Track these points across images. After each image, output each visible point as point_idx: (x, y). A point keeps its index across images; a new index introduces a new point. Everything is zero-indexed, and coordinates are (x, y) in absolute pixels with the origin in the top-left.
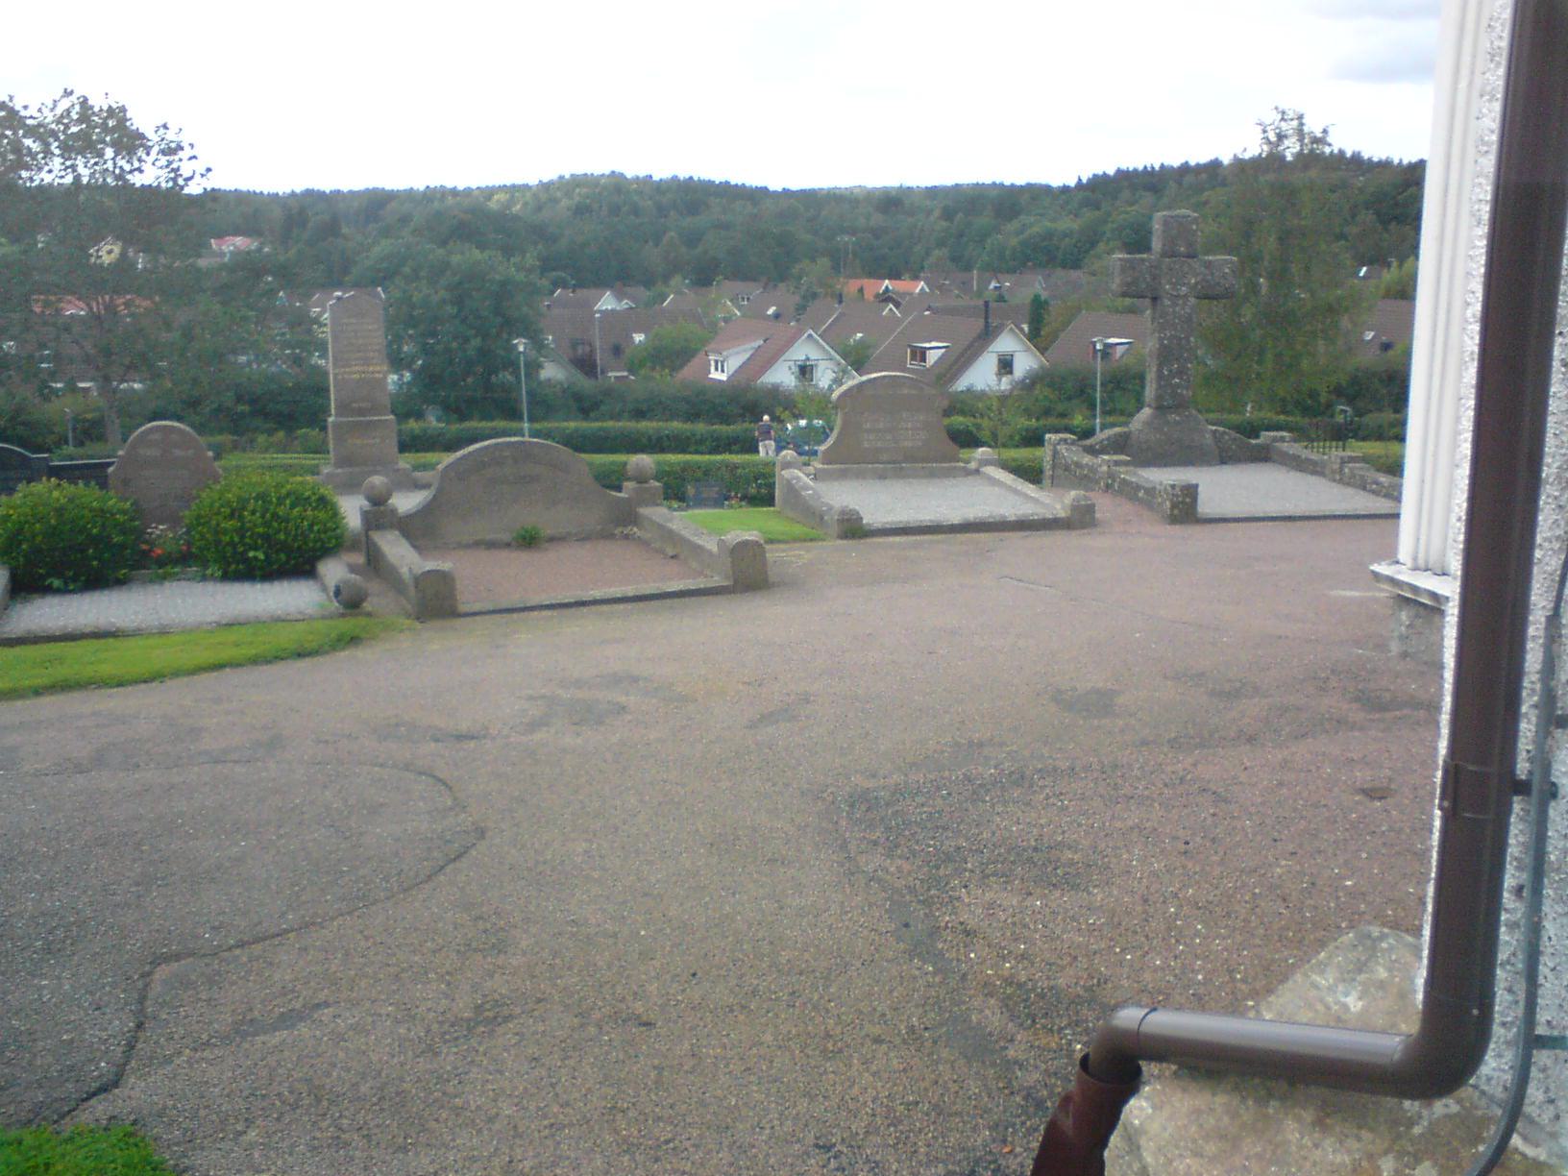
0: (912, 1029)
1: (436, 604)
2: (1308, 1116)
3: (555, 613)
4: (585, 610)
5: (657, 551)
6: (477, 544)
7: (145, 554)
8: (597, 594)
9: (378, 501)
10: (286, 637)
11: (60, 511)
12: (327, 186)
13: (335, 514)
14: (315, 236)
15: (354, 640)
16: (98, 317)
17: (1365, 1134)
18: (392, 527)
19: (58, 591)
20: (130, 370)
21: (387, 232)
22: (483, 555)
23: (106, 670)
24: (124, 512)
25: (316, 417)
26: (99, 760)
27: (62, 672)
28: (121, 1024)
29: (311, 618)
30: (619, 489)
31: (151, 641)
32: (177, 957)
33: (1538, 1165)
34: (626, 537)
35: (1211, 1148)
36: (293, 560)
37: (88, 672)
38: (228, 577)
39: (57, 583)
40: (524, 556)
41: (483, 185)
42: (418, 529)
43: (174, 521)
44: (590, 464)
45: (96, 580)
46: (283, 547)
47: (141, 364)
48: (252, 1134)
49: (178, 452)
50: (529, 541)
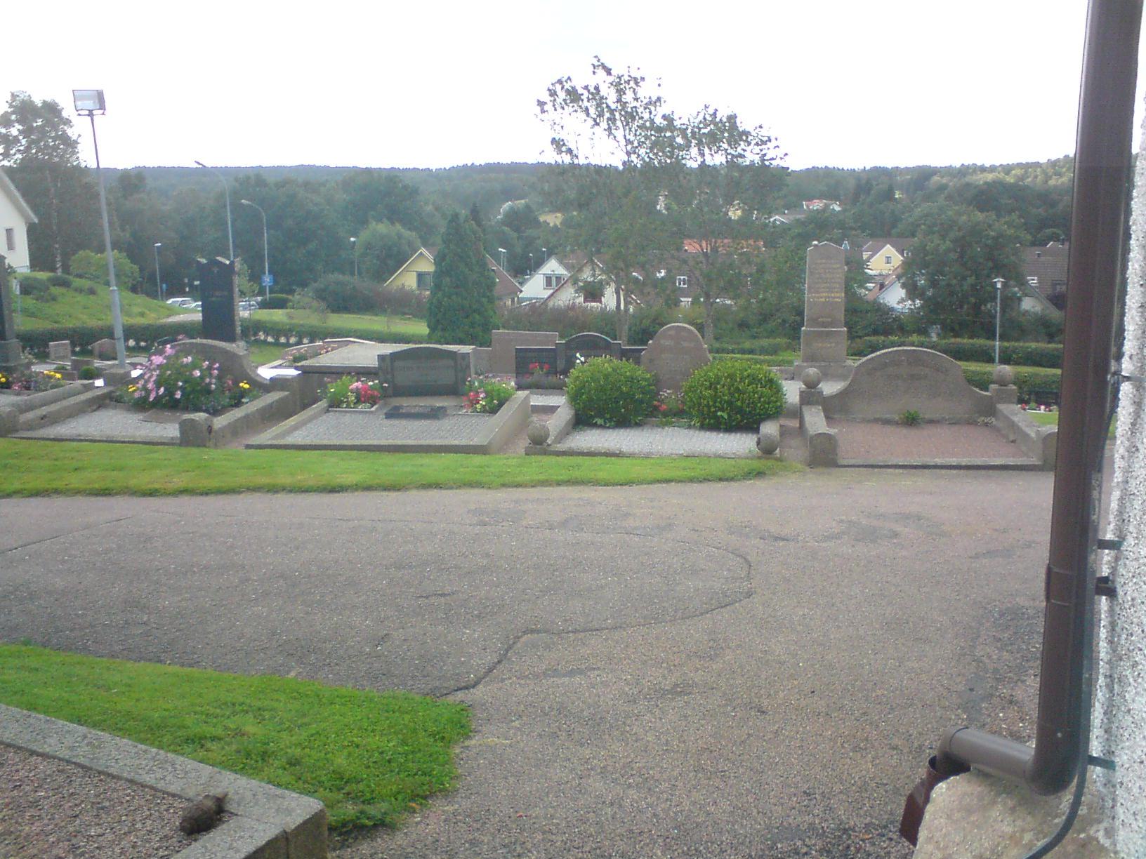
0: (920, 747)
1: (823, 456)
2: (1010, 803)
3: (905, 471)
4: (926, 471)
5: (1003, 436)
6: (876, 420)
7: (656, 408)
8: (939, 461)
9: (811, 385)
10: (716, 468)
11: (607, 376)
12: (889, 164)
13: (778, 390)
14: (874, 202)
15: (760, 474)
16: (706, 254)
17: (1029, 819)
18: (817, 403)
19: (601, 426)
20: (724, 291)
21: (928, 197)
22: (877, 428)
23: (601, 475)
24: (646, 380)
25: (793, 331)
26: (564, 524)
27: (576, 474)
28: (490, 658)
29: (740, 458)
30: (987, 390)
31: (638, 461)
32: (538, 632)
33: (1102, 848)
34: (986, 425)
35: (957, 816)
36: (745, 421)
37: (591, 475)
38: (704, 427)
39: (600, 421)
40: (904, 431)
41: (1005, 163)
42: (834, 408)
43: (677, 388)
44: (965, 372)
45: (622, 422)
46: (740, 411)
47: (731, 287)
48: (517, 724)
49: (685, 344)
50: (911, 421)
